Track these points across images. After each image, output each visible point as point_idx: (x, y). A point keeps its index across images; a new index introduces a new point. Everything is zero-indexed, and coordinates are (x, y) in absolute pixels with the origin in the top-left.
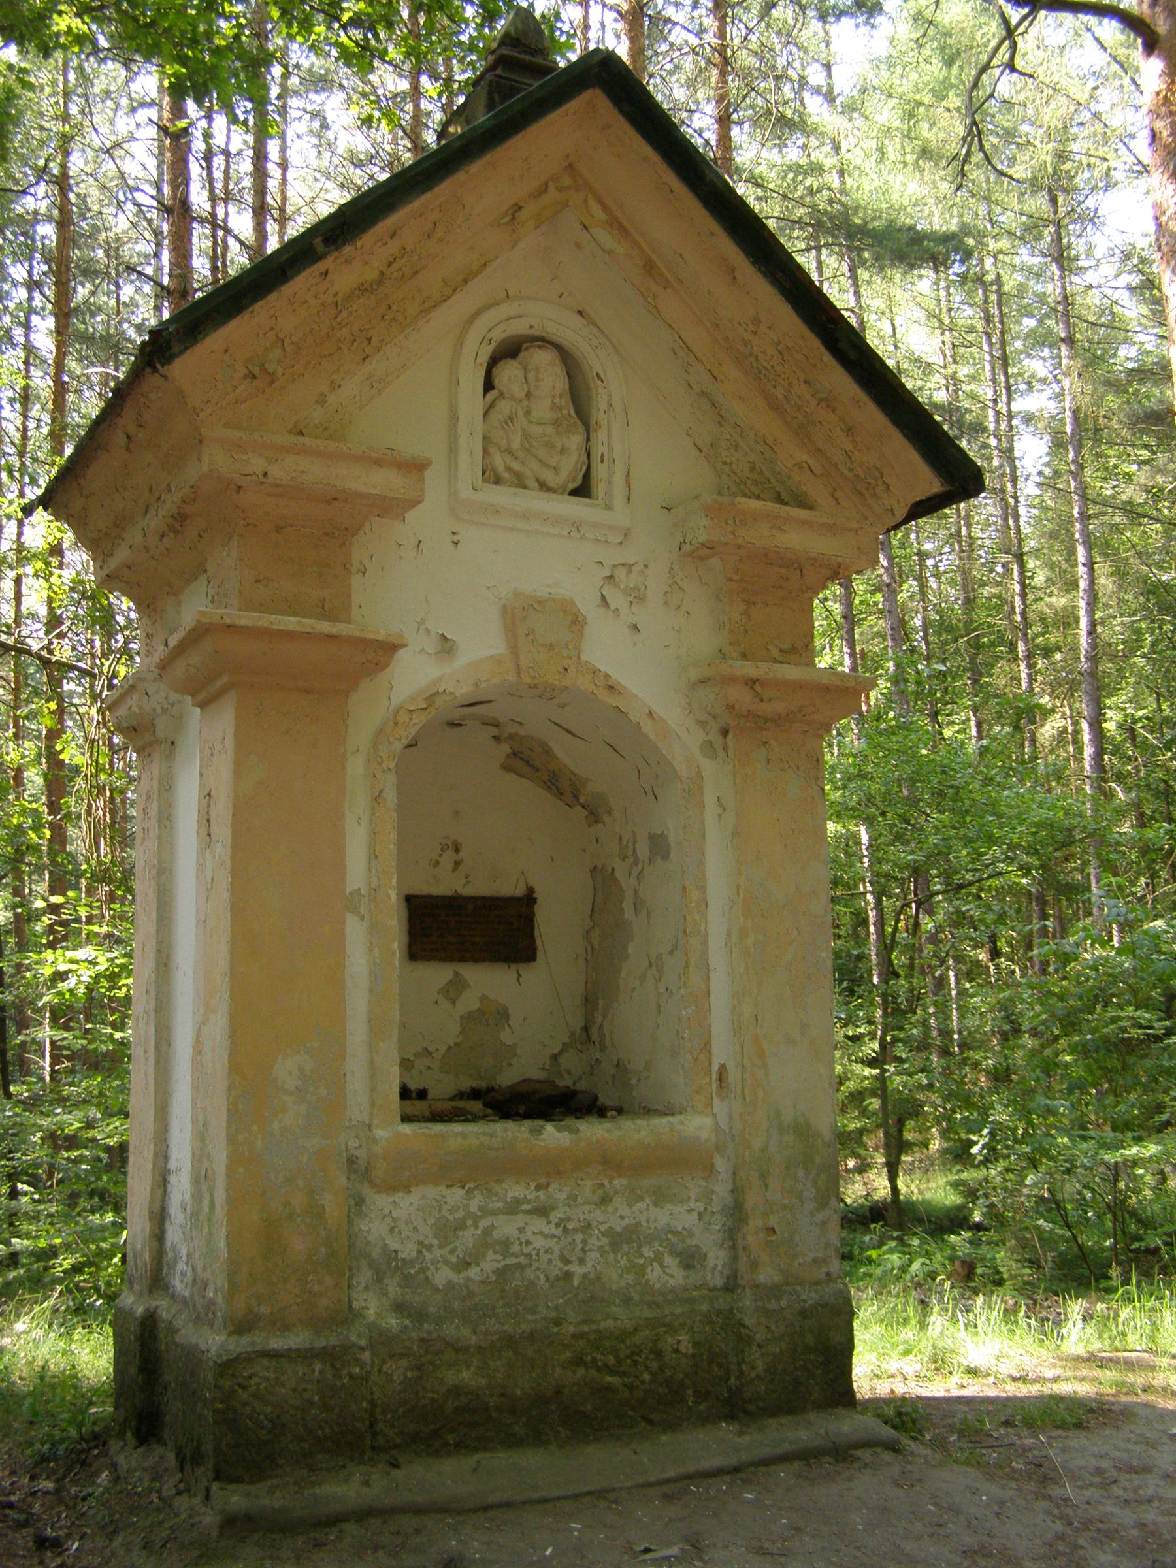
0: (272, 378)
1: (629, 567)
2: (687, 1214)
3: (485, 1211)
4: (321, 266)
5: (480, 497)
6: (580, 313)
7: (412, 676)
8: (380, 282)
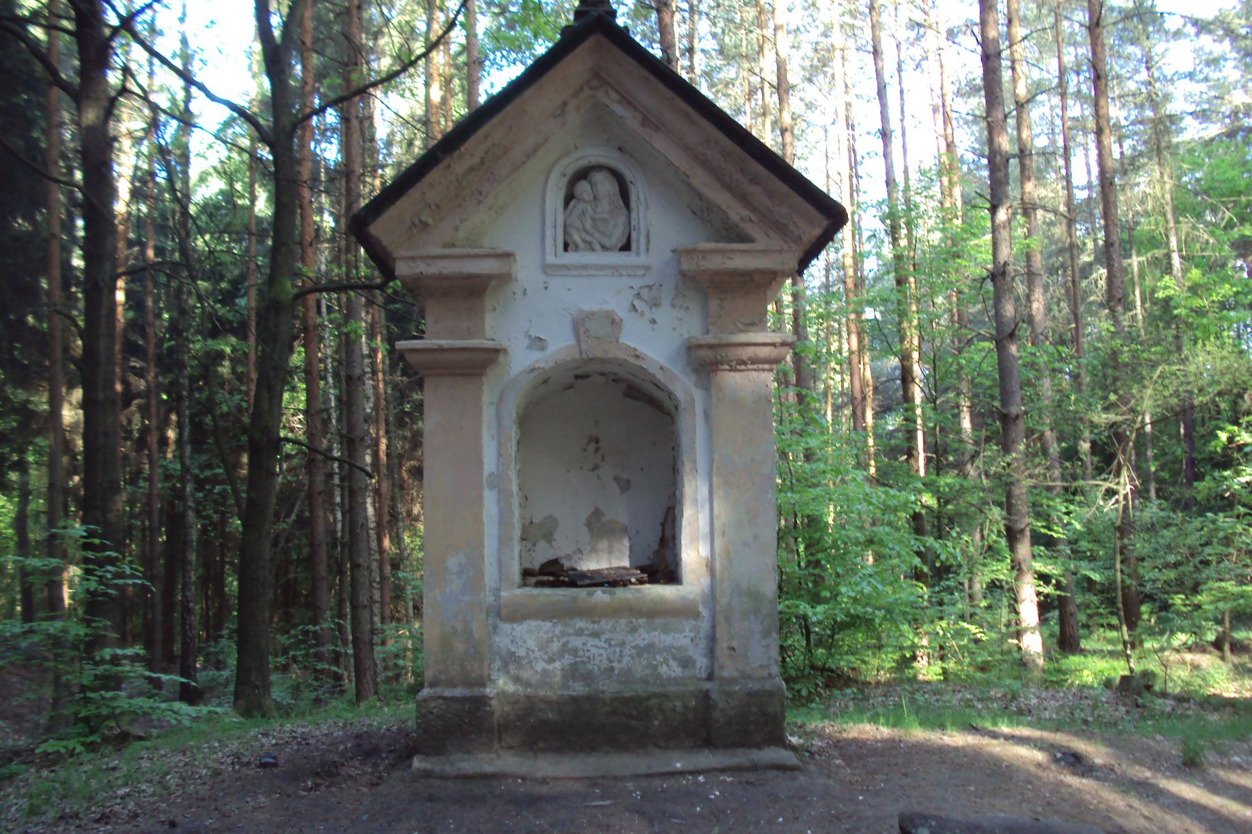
0: (425, 225)
1: (650, 287)
2: (684, 638)
3: (563, 634)
4: (445, 163)
5: (559, 261)
6: (620, 149)
7: (521, 361)
8: (482, 163)
